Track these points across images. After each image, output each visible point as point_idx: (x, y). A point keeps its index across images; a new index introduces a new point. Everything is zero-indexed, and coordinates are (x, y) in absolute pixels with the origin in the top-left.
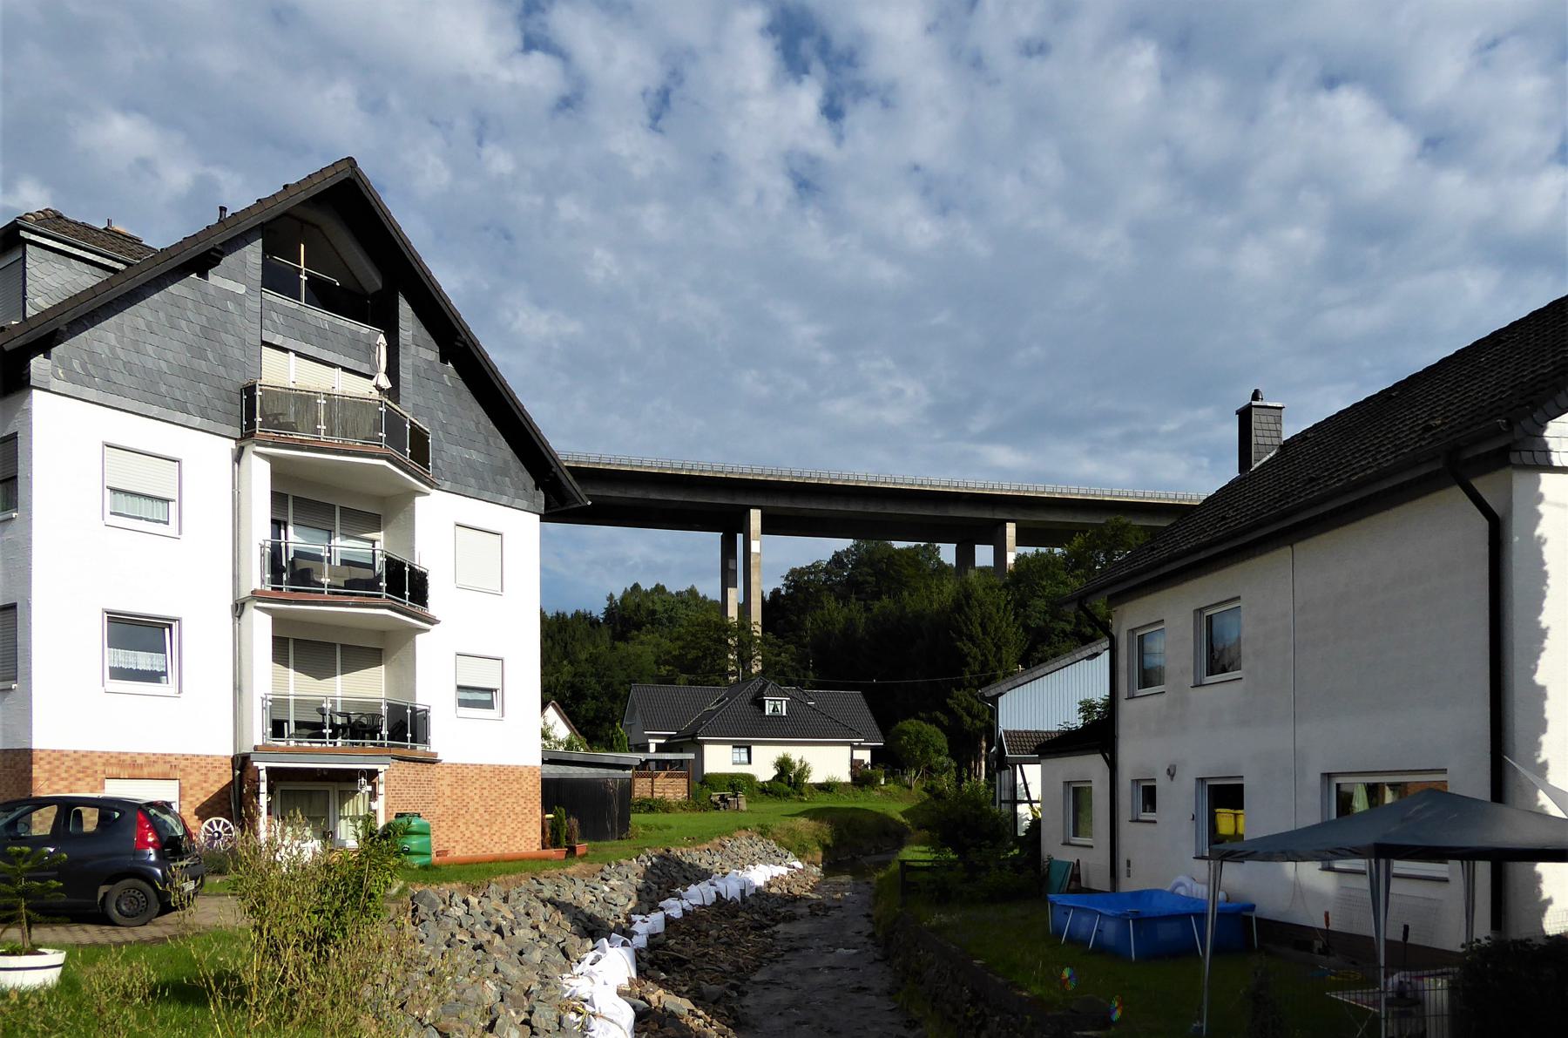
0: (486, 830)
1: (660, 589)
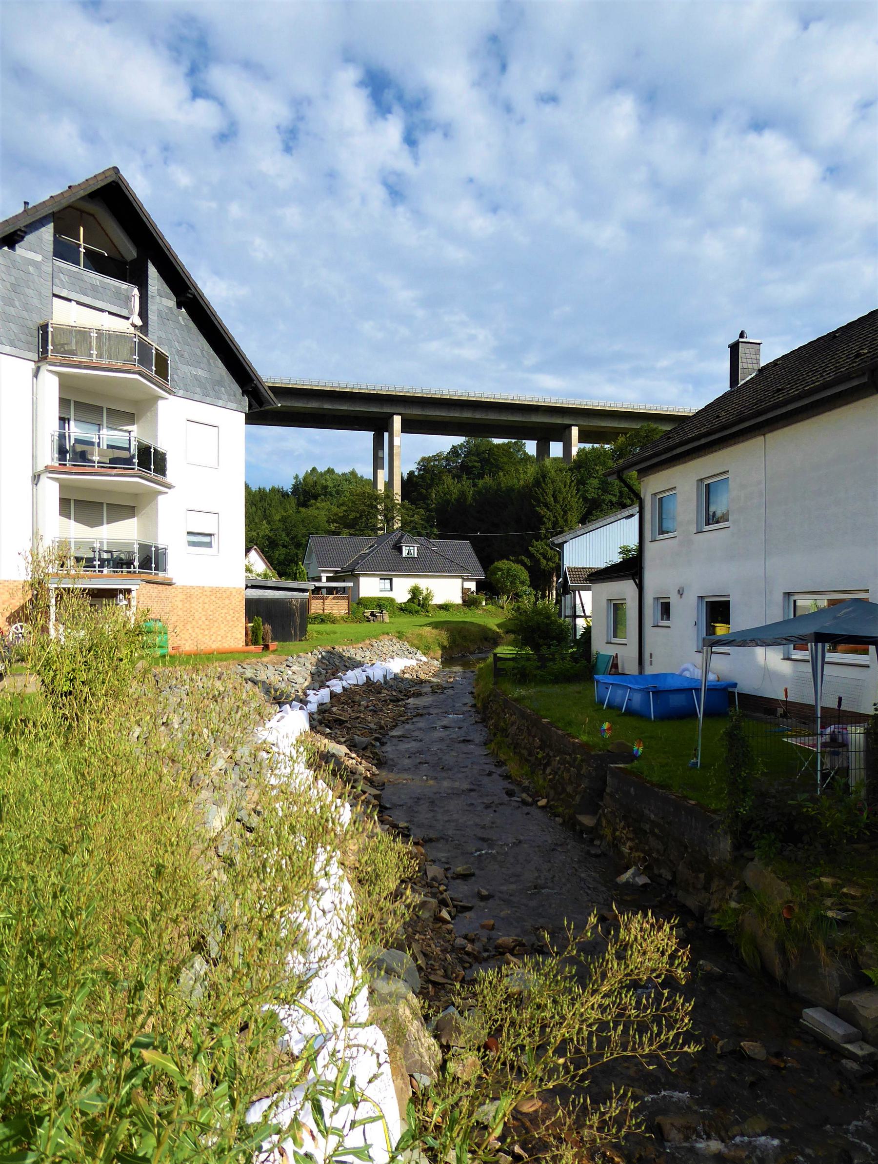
0: (207, 632)
1: (330, 471)
